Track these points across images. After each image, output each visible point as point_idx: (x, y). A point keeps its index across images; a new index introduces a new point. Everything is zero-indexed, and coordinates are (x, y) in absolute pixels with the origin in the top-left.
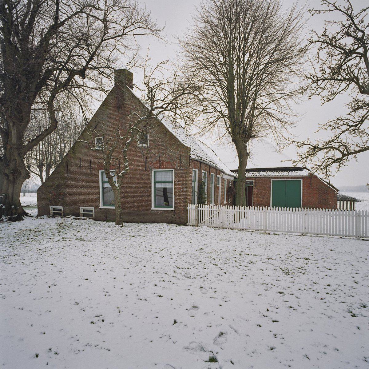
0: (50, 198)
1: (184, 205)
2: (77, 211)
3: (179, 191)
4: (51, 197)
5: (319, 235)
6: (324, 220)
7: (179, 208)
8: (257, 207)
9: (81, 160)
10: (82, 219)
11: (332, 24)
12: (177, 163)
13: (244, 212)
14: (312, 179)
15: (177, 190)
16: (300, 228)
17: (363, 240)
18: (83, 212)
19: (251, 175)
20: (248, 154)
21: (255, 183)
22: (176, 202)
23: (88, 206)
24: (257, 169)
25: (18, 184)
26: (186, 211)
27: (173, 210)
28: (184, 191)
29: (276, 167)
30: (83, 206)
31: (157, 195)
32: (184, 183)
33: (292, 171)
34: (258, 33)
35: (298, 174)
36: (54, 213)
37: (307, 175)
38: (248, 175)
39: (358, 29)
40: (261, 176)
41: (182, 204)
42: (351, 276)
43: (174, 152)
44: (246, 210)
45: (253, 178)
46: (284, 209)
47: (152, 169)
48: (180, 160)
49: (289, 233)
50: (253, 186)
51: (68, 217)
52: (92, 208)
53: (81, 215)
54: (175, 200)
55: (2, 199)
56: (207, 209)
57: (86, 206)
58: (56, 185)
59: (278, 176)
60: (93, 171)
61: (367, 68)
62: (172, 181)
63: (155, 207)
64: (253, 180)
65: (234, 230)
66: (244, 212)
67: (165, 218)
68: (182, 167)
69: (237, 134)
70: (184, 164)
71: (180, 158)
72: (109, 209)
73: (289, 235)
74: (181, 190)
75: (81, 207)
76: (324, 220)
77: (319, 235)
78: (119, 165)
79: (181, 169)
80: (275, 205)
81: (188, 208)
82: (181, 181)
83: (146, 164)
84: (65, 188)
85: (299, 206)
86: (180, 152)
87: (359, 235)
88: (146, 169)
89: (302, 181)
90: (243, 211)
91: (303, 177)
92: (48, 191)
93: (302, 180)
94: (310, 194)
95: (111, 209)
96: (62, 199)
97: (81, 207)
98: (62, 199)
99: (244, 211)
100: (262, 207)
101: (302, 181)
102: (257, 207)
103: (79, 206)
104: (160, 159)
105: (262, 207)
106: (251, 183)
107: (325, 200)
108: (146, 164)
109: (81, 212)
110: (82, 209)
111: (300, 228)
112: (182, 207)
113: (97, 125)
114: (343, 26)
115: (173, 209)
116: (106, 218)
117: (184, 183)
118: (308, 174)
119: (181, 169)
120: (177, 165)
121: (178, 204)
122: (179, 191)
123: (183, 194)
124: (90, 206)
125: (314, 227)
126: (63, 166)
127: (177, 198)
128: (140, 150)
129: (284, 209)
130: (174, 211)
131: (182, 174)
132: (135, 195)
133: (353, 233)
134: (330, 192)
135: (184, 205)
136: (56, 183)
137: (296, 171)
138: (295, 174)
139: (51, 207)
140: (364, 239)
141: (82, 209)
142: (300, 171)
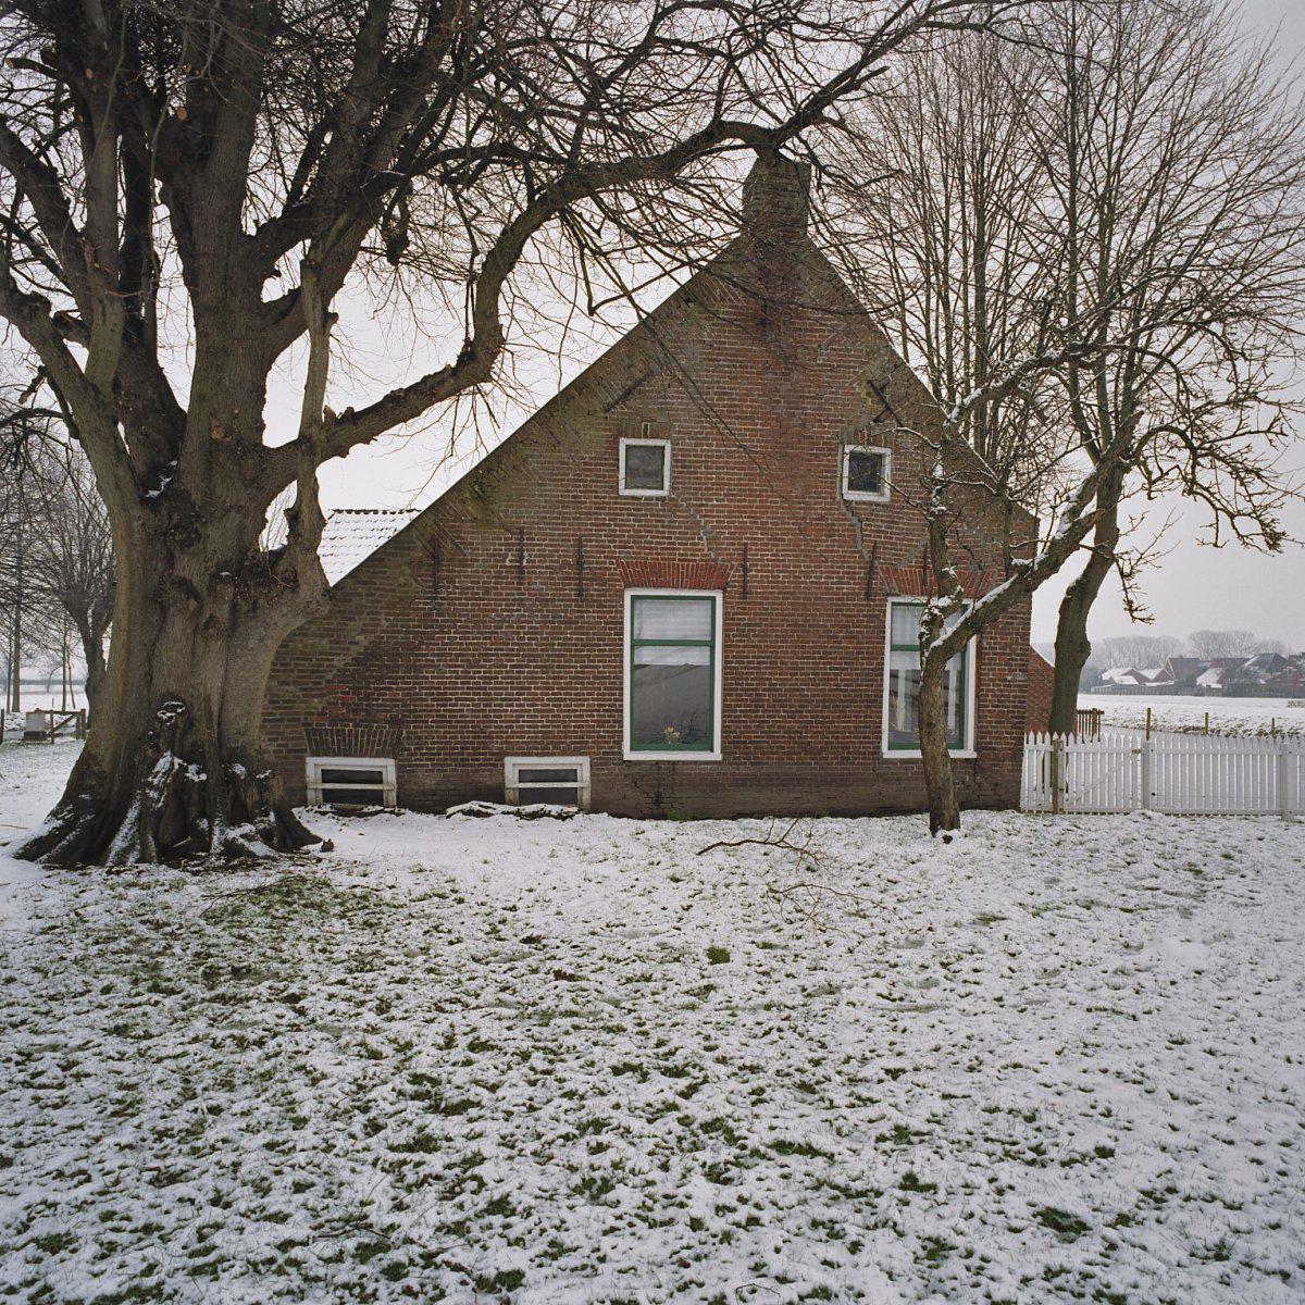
0: (315, 720)
2: (488, 779)
4: (322, 714)
9: (522, 533)
10: (549, 815)
16: (1263, 798)
18: (324, 781)
23: (554, 754)
25: (252, 643)
30: (524, 755)
34: (1087, 161)
36: (325, 791)
43: (986, 536)
47: (725, 591)
51: (466, 806)
52: (582, 765)
53: (509, 795)
54: (979, 718)
55: (175, 724)
57: (542, 755)
58: (354, 650)
60: (593, 590)
61: (642, 322)
62: (632, 647)
72: (674, 763)
75: (509, 761)
78: (746, 570)
83: (871, 571)
84: (418, 669)
88: (868, 595)
92: (294, 683)
95: (684, 763)
96: (394, 722)
97: (509, 761)
98: (394, 722)
103: (501, 756)
104: (745, 560)
108: (871, 571)
109: (509, 784)
110: (512, 766)
111: (1263, 798)
113: (640, 382)
116: (658, 801)
124: (565, 753)
126: (408, 559)
128: (849, 515)
132: (811, 701)
133: (1271, 803)
136: (356, 643)
139: (314, 766)
141: (512, 766)
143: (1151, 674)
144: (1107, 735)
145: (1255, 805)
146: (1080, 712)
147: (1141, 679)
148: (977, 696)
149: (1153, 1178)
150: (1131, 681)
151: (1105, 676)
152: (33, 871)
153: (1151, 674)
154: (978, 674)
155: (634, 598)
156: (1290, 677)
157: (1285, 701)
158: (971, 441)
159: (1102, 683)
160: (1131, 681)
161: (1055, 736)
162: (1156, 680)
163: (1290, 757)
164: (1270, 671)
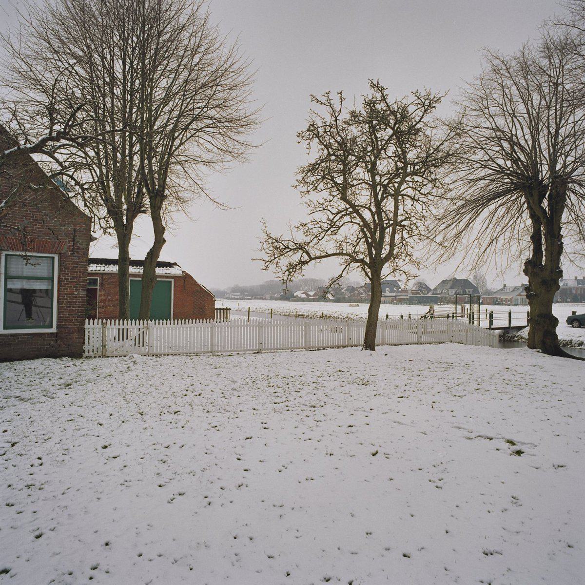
1: (79, 322)
3: (70, 297)
5: (273, 351)
6: (201, 334)
7: (67, 328)
8: (185, 321)
11: (316, 115)
12: (67, 244)
13: (127, 329)
14: (187, 279)
15: (65, 294)
17: (310, 350)
19: (94, 269)
20: (165, 241)
21: (102, 283)
22: (61, 317)
24: (103, 259)
26: (82, 331)
27: (55, 331)
28: (80, 297)
29: (107, 258)
31: (9, 301)
32: (81, 282)
33: (114, 265)
35: (168, 272)
37: (180, 274)
38: (159, 271)
39: (338, 133)
40: (113, 272)
41: (75, 320)
42: (324, 392)
44: (125, 326)
45: (97, 274)
46: (111, 323)
48: (74, 240)
49: (240, 353)
50: (98, 287)
54: (59, 313)
56: (123, 327)
59: (139, 273)
63: (51, 327)
64: (98, 278)
65: (170, 357)
66: (127, 329)
67: (33, 348)
68: (78, 253)
69: (157, 208)
70: (81, 246)
71: (74, 236)
73: (242, 354)
74: (74, 294)
76: (201, 334)
77: (273, 351)
79: (76, 256)
80: (176, 317)
81: (87, 326)
82: (74, 278)
85: (168, 317)
86: (74, 225)
87: (308, 346)
89: (173, 283)
90: (125, 326)
91: (175, 277)
93: (173, 280)
94: (183, 301)
99: (127, 327)
100: (147, 321)
101: (173, 283)
102: (185, 321)
105: (147, 321)
106: (94, 282)
107: (202, 309)
112: (75, 325)
114: (325, 123)
115: (54, 330)
117: (81, 282)
118: (181, 272)
119: (76, 256)
120: (65, 249)
121: (66, 320)
122: (70, 297)
123: (79, 302)
125: (340, 338)
127: (64, 309)
129: (111, 323)
130: (57, 333)
131: (77, 264)
134: (207, 299)
135: (79, 322)
137: (165, 268)
138: (164, 272)
140: (311, 349)
142: (170, 267)
143: (311, 293)
144: (252, 319)
145: (201, 349)
146: (217, 309)
147: (308, 295)
148: (58, 302)
149: (495, 551)
150: (304, 296)
151: (295, 294)
152: (523, 451)
153: (311, 293)
154: (58, 291)
155: (6, 255)
156: (356, 295)
157: (349, 304)
158: (39, 193)
159: (294, 297)
160: (304, 296)
161: (104, 321)
162: (313, 296)
163: (214, 328)
164: (350, 293)
